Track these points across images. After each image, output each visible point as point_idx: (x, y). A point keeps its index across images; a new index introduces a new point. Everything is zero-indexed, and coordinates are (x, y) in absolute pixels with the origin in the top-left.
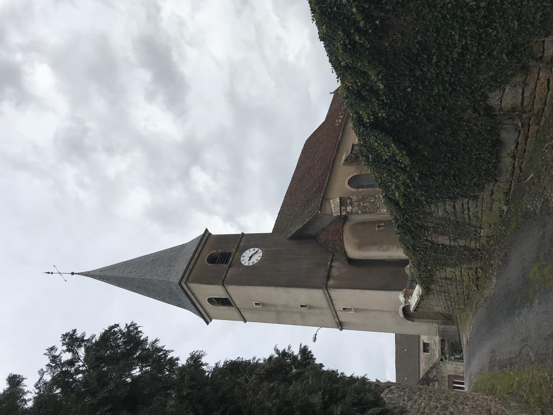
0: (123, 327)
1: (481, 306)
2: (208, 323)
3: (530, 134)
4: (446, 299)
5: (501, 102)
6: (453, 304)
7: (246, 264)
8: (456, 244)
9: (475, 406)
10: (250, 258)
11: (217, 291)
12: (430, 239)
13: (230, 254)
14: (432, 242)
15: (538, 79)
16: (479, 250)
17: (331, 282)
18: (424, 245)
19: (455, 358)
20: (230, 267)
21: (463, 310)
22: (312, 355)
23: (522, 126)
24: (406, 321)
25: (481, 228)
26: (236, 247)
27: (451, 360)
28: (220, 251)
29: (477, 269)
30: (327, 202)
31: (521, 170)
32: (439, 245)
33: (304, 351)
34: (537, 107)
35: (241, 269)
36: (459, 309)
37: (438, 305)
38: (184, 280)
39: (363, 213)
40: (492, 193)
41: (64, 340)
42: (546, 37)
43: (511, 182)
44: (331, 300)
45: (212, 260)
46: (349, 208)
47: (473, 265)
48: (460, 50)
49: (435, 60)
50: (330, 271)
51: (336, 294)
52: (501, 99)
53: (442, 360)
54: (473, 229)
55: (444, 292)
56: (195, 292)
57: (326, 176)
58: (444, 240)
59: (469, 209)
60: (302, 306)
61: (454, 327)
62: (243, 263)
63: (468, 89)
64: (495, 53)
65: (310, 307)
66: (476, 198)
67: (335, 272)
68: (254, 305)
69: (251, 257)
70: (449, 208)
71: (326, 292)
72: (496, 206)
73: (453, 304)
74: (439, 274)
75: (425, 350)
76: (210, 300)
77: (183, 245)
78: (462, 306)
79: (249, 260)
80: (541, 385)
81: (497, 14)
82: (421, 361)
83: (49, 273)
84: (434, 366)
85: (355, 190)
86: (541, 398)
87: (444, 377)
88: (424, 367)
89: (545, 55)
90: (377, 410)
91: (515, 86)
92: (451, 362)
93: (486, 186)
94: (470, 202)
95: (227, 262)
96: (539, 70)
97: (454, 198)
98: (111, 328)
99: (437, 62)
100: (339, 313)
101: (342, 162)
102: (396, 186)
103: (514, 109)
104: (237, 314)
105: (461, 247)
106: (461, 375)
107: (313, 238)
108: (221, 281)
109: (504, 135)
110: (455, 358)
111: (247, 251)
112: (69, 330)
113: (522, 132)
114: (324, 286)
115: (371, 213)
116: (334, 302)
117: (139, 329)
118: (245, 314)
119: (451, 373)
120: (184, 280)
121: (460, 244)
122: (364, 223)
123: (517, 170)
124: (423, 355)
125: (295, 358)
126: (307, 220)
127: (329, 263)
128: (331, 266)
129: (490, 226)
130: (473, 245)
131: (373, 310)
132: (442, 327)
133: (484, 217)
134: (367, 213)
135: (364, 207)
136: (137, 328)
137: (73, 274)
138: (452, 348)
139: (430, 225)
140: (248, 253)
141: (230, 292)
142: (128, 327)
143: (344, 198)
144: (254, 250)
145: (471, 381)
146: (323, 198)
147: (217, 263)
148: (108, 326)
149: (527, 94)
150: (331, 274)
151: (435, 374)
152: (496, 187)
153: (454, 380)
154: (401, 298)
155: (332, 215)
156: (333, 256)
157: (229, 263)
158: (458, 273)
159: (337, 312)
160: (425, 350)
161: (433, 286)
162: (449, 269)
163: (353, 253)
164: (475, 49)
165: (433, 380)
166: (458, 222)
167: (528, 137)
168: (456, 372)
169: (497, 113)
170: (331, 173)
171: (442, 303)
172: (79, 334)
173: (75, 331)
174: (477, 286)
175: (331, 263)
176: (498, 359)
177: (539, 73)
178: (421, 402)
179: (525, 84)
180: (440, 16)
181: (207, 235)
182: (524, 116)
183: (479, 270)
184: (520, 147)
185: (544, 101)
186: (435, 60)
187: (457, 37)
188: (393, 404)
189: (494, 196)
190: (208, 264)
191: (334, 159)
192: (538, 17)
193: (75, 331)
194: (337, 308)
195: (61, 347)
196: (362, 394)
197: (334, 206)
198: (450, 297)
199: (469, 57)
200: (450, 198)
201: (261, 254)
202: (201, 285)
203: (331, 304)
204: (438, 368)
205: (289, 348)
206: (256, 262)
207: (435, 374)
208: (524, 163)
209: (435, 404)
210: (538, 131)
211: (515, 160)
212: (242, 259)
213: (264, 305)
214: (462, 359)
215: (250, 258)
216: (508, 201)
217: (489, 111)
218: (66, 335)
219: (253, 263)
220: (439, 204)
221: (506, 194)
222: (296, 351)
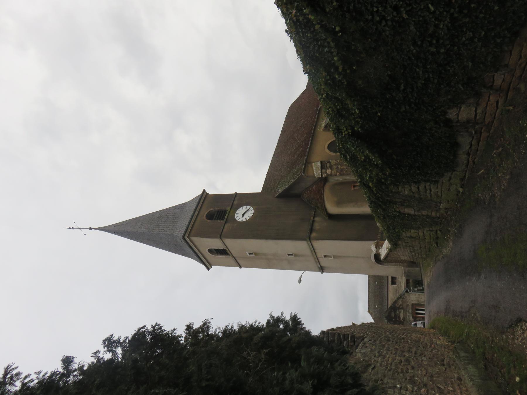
0: (150, 328)
1: (439, 260)
2: (208, 269)
3: (481, 139)
4: (411, 252)
5: (458, 116)
6: (417, 254)
7: (240, 220)
8: (420, 213)
9: (432, 356)
10: (244, 215)
11: (216, 243)
12: (397, 210)
13: (224, 212)
14: (400, 212)
15: (489, 100)
16: (439, 218)
17: (314, 235)
18: (393, 214)
19: (418, 290)
20: (226, 223)
21: (425, 259)
22: (301, 321)
23: (476, 133)
24: (377, 264)
25: (440, 203)
26: (231, 205)
27: (415, 291)
28: (216, 209)
29: (437, 231)
30: (309, 165)
31: (474, 163)
32: (406, 214)
33: (294, 318)
34: (487, 120)
35: (236, 225)
36: (422, 258)
37: (404, 254)
38: (187, 234)
39: (341, 175)
40: (450, 179)
41: (105, 343)
42: (496, 72)
43: (466, 171)
44: (314, 249)
45: (210, 216)
46: (329, 171)
47: (434, 228)
48: (423, 82)
49: (402, 87)
50: (312, 225)
51: (317, 244)
52: (458, 115)
53: (407, 292)
54: (434, 204)
55: (410, 246)
56: (196, 244)
57: (308, 141)
58: (410, 211)
59: (430, 190)
60: (289, 255)
61: (417, 269)
62: (237, 219)
63: (430, 108)
64: (452, 84)
65: (296, 255)
66: (436, 182)
67: (317, 226)
68: (248, 254)
69: (244, 214)
70: (414, 189)
71: (309, 243)
72: (453, 188)
73: (417, 254)
74: (405, 234)
75: (393, 283)
76: (210, 251)
77: (184, 203)
78: (424, 256)
79: (243, 217)
80: (484, 342)
81: (454, 56)
82: (389, 292)
83: (70, 228)
84: (401, 297)
85: (334, 154)
86: (484, 354)
87: (408, 305)
88: (392, 297)
89: (495, 84)
90: (355, 391)
91: (469, 106)
92: (414, 293)
93: (446, 174)
94: (432, 185)
95: (223, 219)
96: (490, 94)
97: (418, 182)
98: (140, 329)
99: (404, 90)
100: (321, 260)
101: (323, 128)
102: (370, 177)
103: (468, 121)
104: (232, 261)
105: (424, 216)
106: (423, 303)
107: (298, 197)
108: (219, 236)
109: (460, 139)
110: (418, 290)
111: (241, 209)
112: (107, 335)
113: (475, 137)
114: (308, 240)
115: (348, 175)
116: (316, 251)
117: (163, 328)
118: (240, 262)
119: (414, 302)
120: (187, 234)
121: (423, 213)
122: (342, 183)
123: (471, 163)
124: (391, 287)
125: (286, 323)
126: (292, 181)
127: (312, 218)
128: (313, 221)
129: (448, 201)
130: (434, 214)
131: (349, 257)
132: (407, 269)
133: (443, 196)
134: (344, 175)
135: (342, 170)
136: (161, 328)
137: (90, 229)
138: (415, 283)
139: (397, 200)
140: (241, 211)
141: (227, 244)
142: (153, 327)
143: (324, 162)
144: (246, 208)
145: (430, 317)
146: (306, 162)
147: (215, 219)
148: (138, 328)
149: (479, 111)
150: (313, 228)
151: (401, 303)
152: (453, 175)
153: (417, 311)
154: (373, 248)
155: (314, 177)
156: (315, 212)
157: (225, 219)
158: (421, 234)
159: (319, 259)
160: (393, 283)
161: (400, 242)
162: (413, 231)
163: (332, 209)
164: (436, 81)
165: (399, 308)
166: (421, 199)
167: (480, 141)
168: (418, 301)
169: (454, 124)
170: (312, 139)
171: (407, 254)
172: (115, 338)
173: (112, 335)
174: (437, 244)
175: (314, 218)
176: (452, 308)
177: (489, 97)
178: (389, 358)
179: (478, 104)
180: (407, 58)
181: (205, 195)
182: (477, 127)
183: (439, 232)
184: (473, 148)
185: (493, 116)
186: (402, 87)
187: (421, 72)
188: (366, 361)
189: (452, 181)
190: (206, 220)
191: (315, 126)
192: (489, 59)
193: (112, 335)
194: (319, 256)
195: (102, 349)
196: (343, 378)
197: (316, 169)
198: (414, 250)
199: (431, 86)
200: (415, 182)
201: (253, 212)
202: (202, 239)
203: (313, 252)
204: (403, 298)
205: (282, 314)
206: (248, 218)
207: (401, 303)
208: (477, 159)
209: (400, 358)
210: (488, 136)
211: (469, 156)
212: (236, 215)
213: (256, 254)
214: (423, 290)
215: (244, 215)
216: (463, 185)
217: (448, 123)
218: (106, 339)
219: (245, 219)
220: (406, 186)
221: (462, 180)
222: (288, 318)
